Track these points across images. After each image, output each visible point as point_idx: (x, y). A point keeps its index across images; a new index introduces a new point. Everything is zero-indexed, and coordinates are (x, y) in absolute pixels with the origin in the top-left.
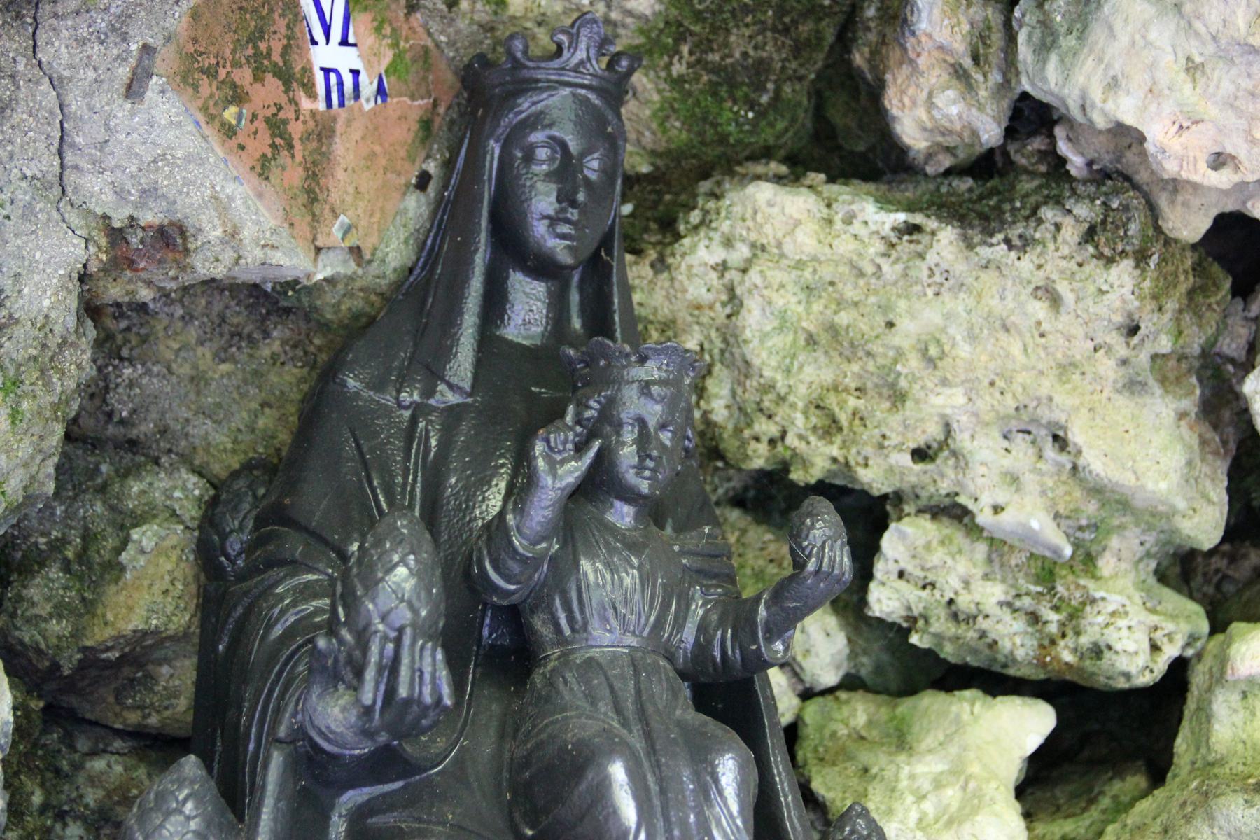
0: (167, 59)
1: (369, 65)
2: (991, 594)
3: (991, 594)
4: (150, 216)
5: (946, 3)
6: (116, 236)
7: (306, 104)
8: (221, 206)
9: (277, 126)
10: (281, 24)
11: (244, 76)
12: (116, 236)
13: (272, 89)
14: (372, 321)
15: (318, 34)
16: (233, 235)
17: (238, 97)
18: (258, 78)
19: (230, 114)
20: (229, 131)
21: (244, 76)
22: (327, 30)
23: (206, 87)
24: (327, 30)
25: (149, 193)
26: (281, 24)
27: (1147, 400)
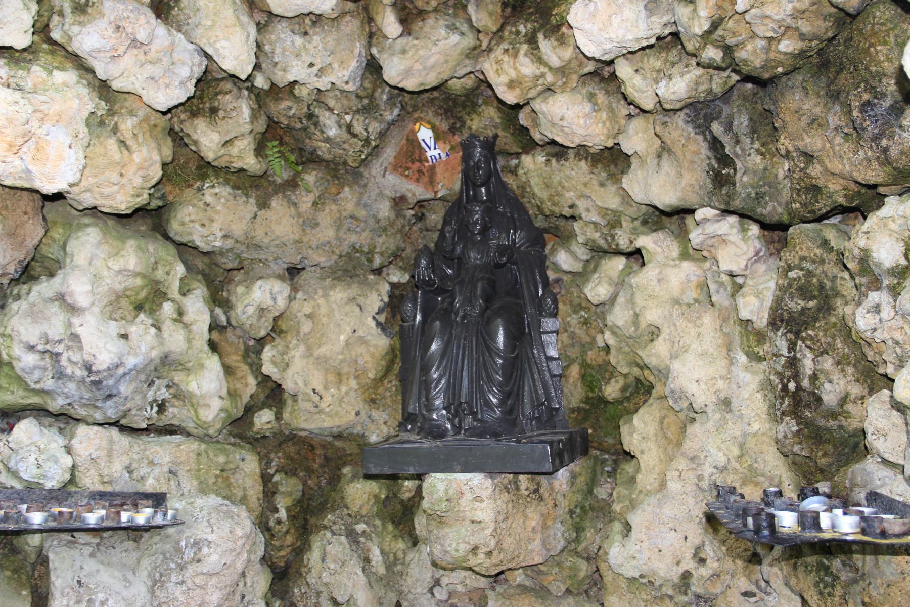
0: (390, 168)
1: (443, 151)
2: (597, 235)
3: (597, 235)
4: (398, 195)
5: (505, 5)
6: (394, 200)
7: (426, 164)
8: (410, 190)
9: (420, 171)
10: (417, 151)
11: (410, 165)
12: (394, 200)
13: (417, 164)
14: (265, 437)
15: (427, 149)
16: (414, 195)
17: (408, 169)
18: (413, 163)
19: (407, 173)
20: (407, 176)
21: (410, 165)
22: (430, 148)
23: (400, 170)
24: (430, 148)
25: (396, 191)
26: (417, 151)
27: (556, 96)
